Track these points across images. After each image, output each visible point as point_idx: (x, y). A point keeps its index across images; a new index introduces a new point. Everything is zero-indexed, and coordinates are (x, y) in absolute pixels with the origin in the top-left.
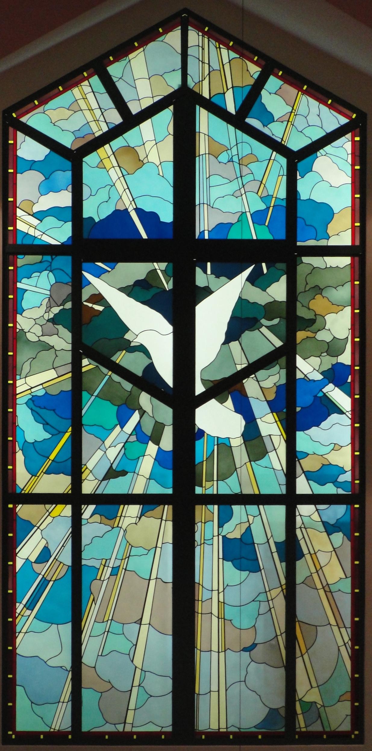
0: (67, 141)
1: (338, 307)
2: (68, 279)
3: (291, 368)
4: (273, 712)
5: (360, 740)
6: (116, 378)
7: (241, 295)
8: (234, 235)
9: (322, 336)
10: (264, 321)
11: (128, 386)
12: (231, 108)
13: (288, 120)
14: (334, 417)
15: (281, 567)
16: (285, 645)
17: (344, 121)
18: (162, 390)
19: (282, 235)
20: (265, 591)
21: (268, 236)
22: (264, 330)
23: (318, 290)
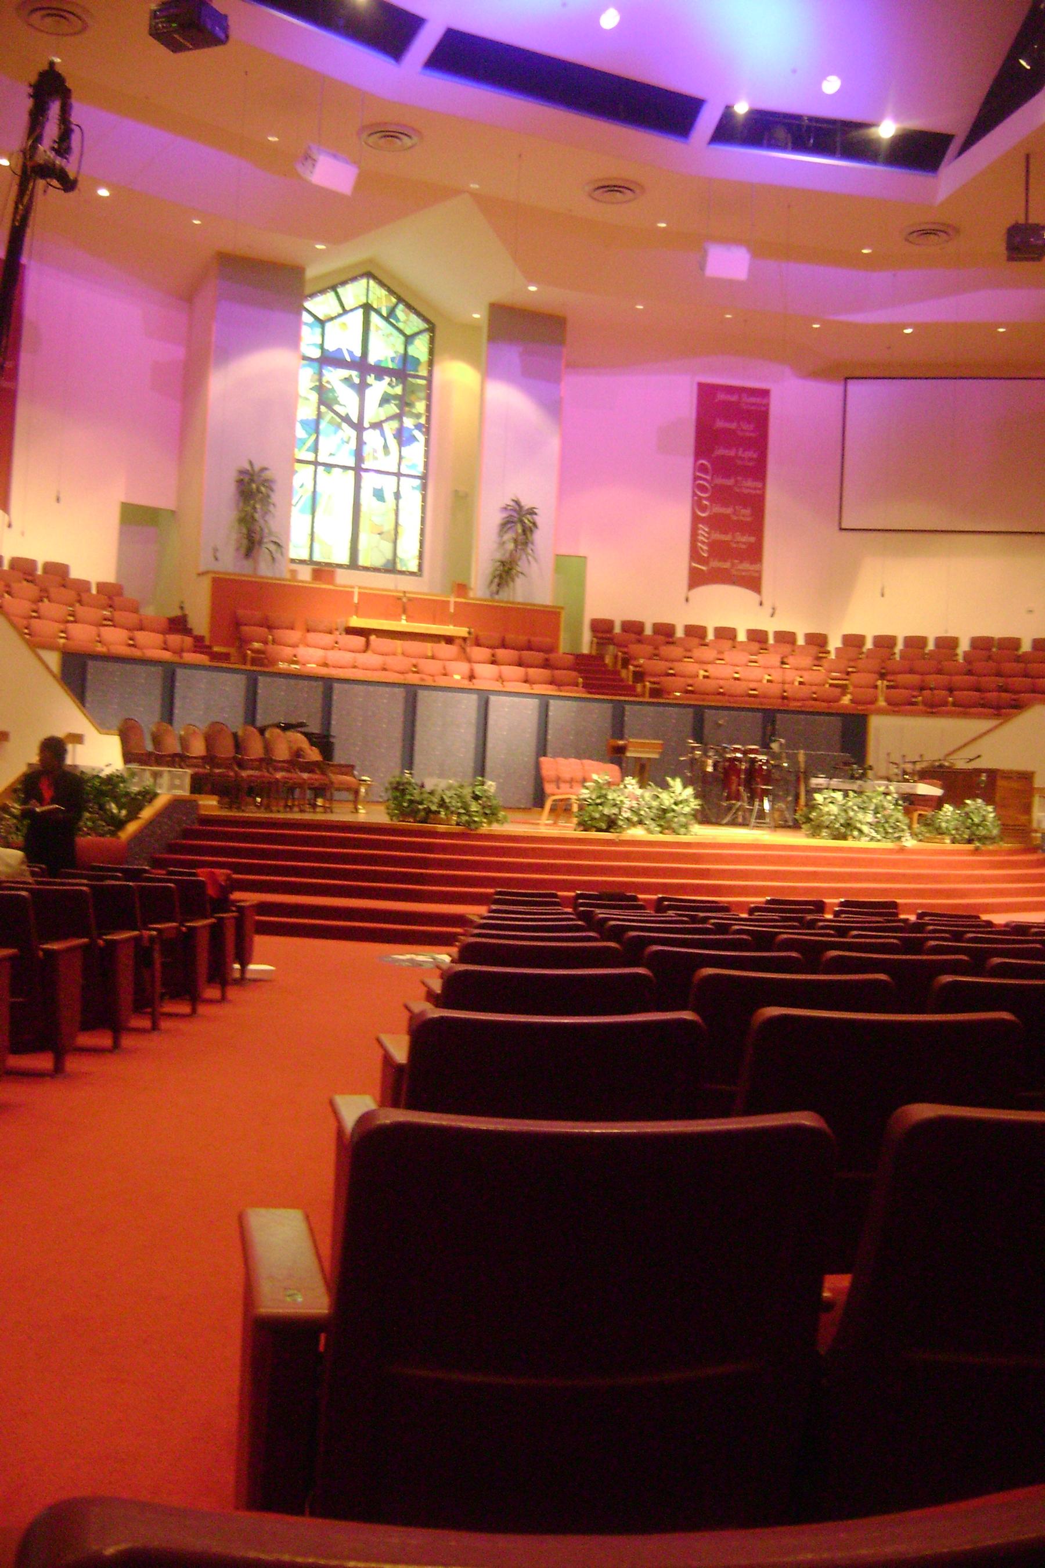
0: (321, 317)
1: (420, 399)
2: (316, 372)
3: (401, 422)
4: (388, 561)
5: (421, 576)
6: (335, 416)
7: (963, 842)
8: (383, 365)
9: (414, 411)
10: (393, 402)
11: (339, 420)
12: (385, 314)
13: (405, 322)
14: (416, 444)
15: (394, 501)
16: (327, 1265)
17: (427, 326)
18: (865, 251)
19: (401, 367)
20: (395, 478)
21: (395, 367)
22: (393, 405)
23: (413, 392)
